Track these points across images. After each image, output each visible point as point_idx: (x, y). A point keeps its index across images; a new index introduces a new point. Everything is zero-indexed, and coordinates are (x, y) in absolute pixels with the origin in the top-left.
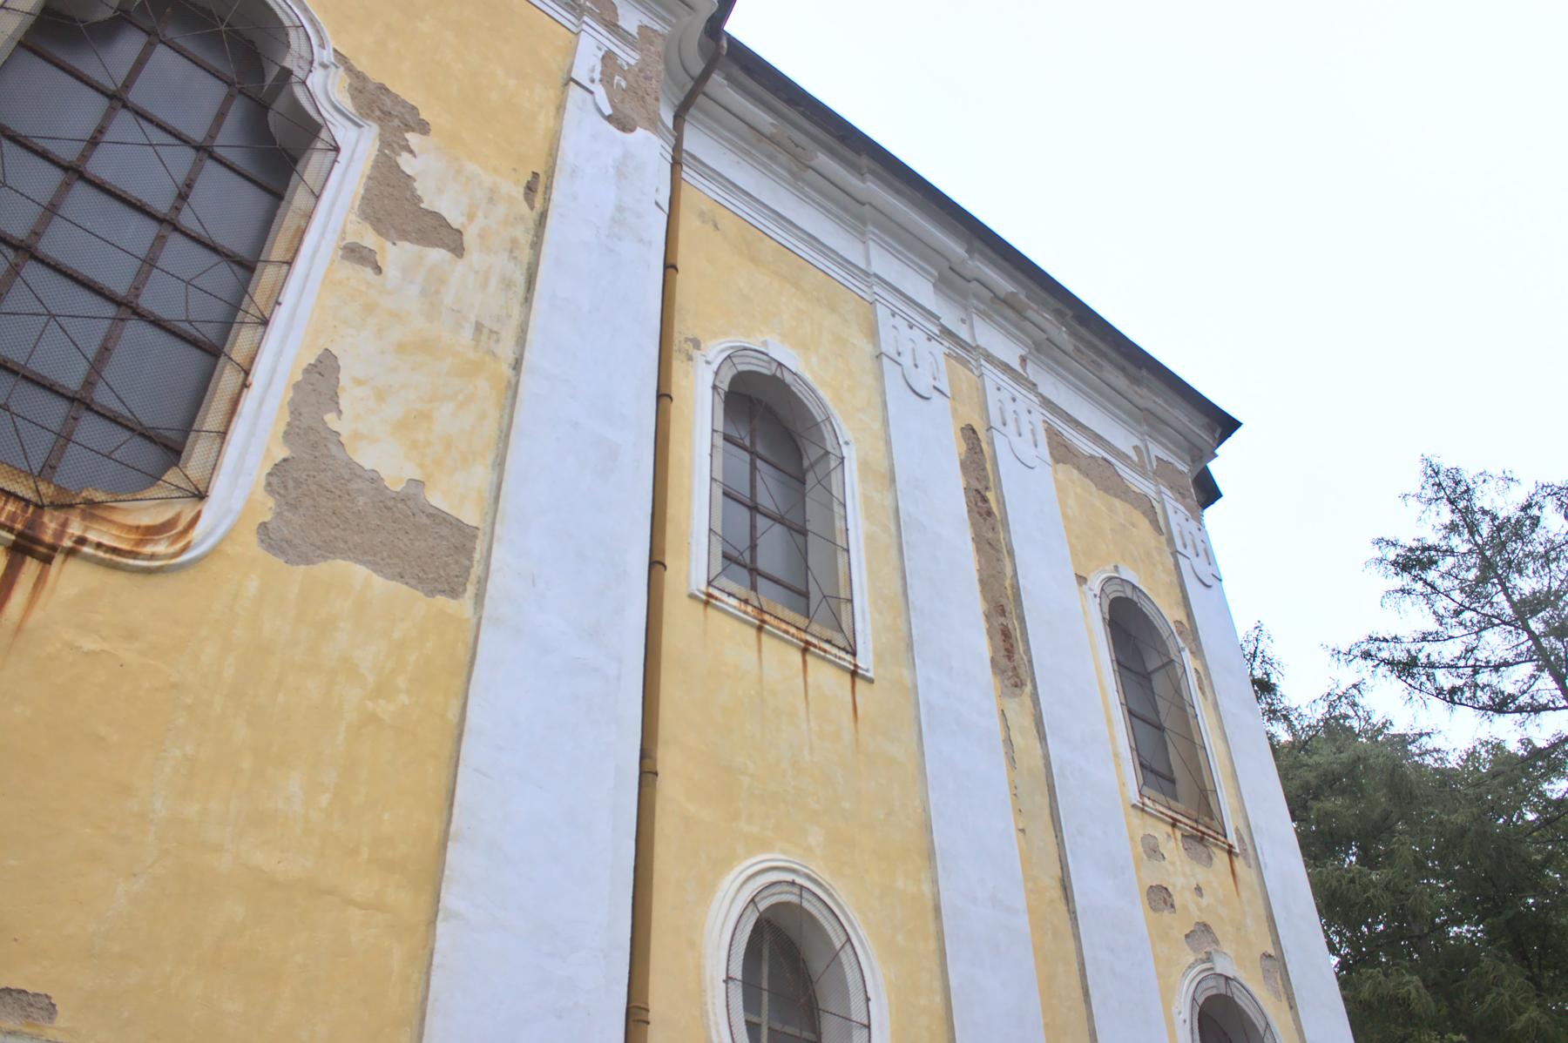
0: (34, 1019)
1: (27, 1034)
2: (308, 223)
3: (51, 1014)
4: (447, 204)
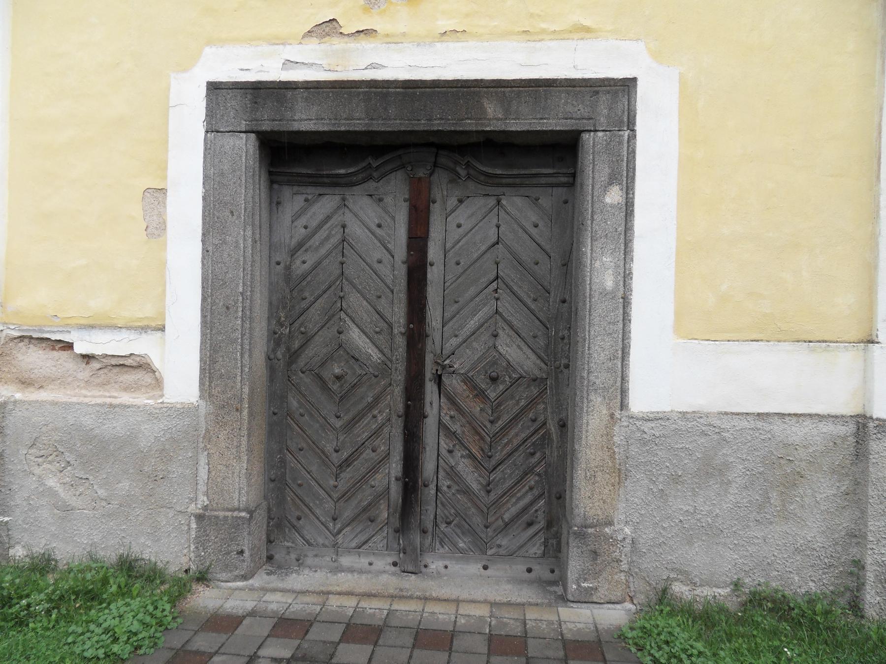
2: (574, 179)
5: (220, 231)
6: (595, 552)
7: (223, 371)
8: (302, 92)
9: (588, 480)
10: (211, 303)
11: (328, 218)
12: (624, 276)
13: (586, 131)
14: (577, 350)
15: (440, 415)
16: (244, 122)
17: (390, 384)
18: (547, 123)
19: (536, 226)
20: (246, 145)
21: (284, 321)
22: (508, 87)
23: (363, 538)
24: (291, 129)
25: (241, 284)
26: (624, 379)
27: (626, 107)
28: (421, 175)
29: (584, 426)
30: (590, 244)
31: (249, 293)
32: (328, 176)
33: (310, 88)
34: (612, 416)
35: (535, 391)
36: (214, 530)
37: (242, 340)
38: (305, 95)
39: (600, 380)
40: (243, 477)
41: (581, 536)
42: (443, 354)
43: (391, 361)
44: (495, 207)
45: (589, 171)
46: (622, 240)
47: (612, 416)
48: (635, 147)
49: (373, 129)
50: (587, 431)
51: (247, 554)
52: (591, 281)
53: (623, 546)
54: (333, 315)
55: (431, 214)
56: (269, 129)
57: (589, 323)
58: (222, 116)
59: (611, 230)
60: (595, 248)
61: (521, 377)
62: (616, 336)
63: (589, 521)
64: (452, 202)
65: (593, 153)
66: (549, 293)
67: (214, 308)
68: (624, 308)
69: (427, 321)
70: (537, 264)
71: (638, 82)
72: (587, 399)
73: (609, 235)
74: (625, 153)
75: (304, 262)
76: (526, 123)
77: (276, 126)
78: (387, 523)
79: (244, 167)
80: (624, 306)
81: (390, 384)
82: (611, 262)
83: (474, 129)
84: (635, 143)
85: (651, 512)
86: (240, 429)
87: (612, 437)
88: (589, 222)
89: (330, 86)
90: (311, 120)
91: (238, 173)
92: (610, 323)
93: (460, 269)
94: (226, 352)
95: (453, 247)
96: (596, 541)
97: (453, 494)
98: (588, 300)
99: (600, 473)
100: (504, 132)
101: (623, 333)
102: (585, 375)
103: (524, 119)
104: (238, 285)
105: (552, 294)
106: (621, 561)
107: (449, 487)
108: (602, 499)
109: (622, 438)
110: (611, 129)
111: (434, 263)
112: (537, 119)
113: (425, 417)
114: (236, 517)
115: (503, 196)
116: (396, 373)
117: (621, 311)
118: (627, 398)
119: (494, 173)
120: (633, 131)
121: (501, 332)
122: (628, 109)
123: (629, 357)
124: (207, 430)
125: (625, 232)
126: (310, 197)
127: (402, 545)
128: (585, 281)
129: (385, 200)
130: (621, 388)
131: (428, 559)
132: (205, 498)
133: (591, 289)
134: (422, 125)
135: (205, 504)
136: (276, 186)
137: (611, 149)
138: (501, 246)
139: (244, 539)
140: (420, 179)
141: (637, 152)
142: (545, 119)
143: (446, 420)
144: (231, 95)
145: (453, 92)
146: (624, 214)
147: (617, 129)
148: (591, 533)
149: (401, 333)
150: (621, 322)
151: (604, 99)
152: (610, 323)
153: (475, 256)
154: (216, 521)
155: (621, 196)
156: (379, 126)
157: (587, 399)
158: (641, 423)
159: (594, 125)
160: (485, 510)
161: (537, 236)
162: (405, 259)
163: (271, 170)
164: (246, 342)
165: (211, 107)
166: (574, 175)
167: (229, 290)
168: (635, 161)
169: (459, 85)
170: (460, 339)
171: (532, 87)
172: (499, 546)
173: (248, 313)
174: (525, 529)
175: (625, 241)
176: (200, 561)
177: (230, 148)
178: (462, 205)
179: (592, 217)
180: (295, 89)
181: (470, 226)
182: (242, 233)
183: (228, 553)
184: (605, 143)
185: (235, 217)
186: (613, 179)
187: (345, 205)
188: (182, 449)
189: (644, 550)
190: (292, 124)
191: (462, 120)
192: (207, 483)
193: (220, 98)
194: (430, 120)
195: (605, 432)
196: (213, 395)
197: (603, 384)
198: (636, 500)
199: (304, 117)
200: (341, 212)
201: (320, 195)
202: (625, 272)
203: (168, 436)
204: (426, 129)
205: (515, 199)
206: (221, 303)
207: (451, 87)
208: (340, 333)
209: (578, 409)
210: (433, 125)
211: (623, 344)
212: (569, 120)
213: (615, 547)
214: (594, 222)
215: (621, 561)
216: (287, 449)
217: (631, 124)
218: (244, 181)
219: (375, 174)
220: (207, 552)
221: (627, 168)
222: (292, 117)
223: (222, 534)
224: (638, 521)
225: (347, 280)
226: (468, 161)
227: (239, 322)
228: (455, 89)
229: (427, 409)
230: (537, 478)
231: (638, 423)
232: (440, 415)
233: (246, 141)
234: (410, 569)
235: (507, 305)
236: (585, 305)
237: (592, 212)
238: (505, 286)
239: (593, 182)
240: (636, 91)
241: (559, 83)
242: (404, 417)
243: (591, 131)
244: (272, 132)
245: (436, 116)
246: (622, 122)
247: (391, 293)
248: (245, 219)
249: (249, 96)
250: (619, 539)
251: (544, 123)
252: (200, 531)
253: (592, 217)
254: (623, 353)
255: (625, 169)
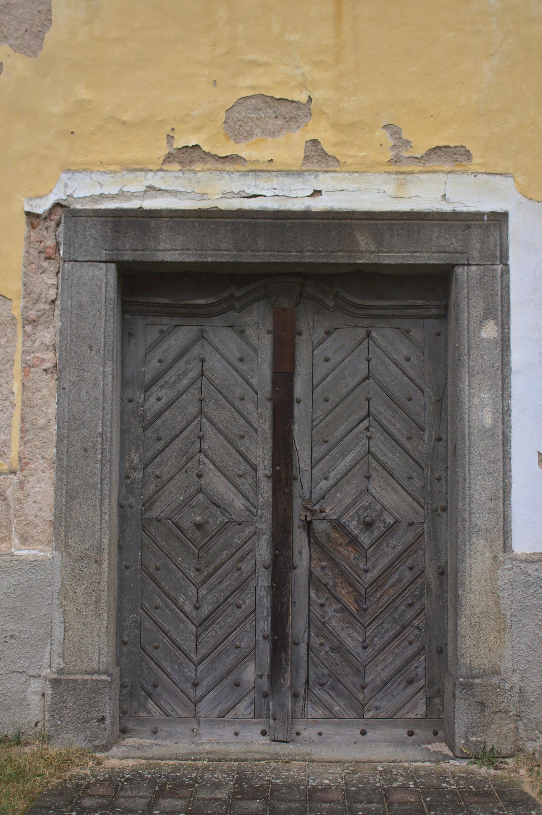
0: (459, 162)
1: (458, 171)
2: (446, 311)
3: (469, 157)
4: (386, 134)
5: (77, 367)
6: (482, 704)
7: (80, 519)
8: (167, 221)
9: (473, 628)
10: (67, 445)
11: (185, 351)
12: (503, 413)
13: (459, 265)
14: (458, 491)
15: (310, 566)
16: (105, 252)
17: (255, 533)
18: (420, 256)
19: (408, 360)
20: (106, 275)
21: (137, 464)
22: (380, 220)
23: (225, 706)
24: (155, 259)
25: (100, 424)
26: (506, 519)
27: (498, 241)
28: (286, 305)
29: (467, 570)
30: (467, 380)
31: (109, 434)
32: (186, 306)
33: (175, 217)
34: (495, 557)
35: (410, 537)
36: (72, 695)
37: (101, 485)
38: (170, 224)
39: (482, 521)
40: (103, 635)
41: (468, 687)
42: (313, 498)
43: (255, 507)
44: (364, 340)
45: (464, 305)
46: (499, 376)
47: (495, 557)
48: (509, 281)
49: (242, 261)
50: (470, 576)
51: (108, 721)
52: (469, 418)
53: (510, 695)
54: (192, 458)
55: (297, 348)
56: (131, 259)
57: (469, 462)
58: (81, 245)
59: (488, 366)
60: (472, 385)
61: (397, 522)
62: (496, 475)
63: (475, 672)
64: (319, 334)
65: (467, 287)
66: (424, 431)
67: (70, 450)
68: (503, 446)
69: (294, 462)
70: (410, 400)
71: (509, 217)
72: (470, 542)
73: (486, 371)
74: (499, 288)
75: (159, 399)
76: (399, 256)
77: (139, 256)
78: (254, 687)
79: (104, 299)
80: (503, 444)
81: (255, 533)
82: (489, 398)
83: (347, 261)
84: (509, 278)
85: (538, 659)
86: (99, 583)
87: (496, 581)
88: (466, 358)
89: (196, 216)
90: (177, 250)
91: (98, 305)
92: (490, 462)
93: (328, 406)
94: (84, 498)
95: (321, 383)
96: (483, 692)
97: (327, 653)
98: (467, 437)
99: (484, 620)
100: (377, 264)
101: (504, 471)
102: (467, 516)
103: (397, 252)
104: (97, 425)
105: (427, 431)
106: (510, 712)
107: (322, 645)
108: (488, 647)
109: (506, 581)
110: (484, 263)
111: (301, 400)
112: (410, 252)
113: (294, 568)
114: (97, 680)
115: (373, 328)
116: (261, 520)
117: (501, 449)
118: (510, 540)
119: (364, 304)
120: (506, 265)
121: (374, 474)
122: (501, 243)
123: (510, 497)
124: (63, 585)
125: (502, 368)
126: (165, 328)
127: (272, 711)
128: (463, 418)
129: (247, 332)
130: (504, 529)
131: (299, 727)
132: (61, 661)
133: (469, 427)
134: (293, 257)
135: (61, 667)
136: (128, 317)
137: (485, 283)
138: (372, 381)
139: (105, 704)
140: (284, 309)
141: (511, 286)
142: (418, 252)
143: (317, 572)
144: (91, 223)
145: (324, 224)
146: (500, 349)
147: (490, 263)
148: (478, 684)
149: (267, 477)
150: (501, 460)
151: (476, 234)
152: (490, 462)
153: (345, 391)
154: (74, 686)
155: (497, 331)
156: (247, 257)
157: (470, 542)
158: (524, 565)
159: (468, 259)
160: (362, 668)
161: (410, 370)
162: (269, 396)
163: (126, 299)
164: (106, 487)
165: (68, 235)
166: (446, 307)
167: (88, 431)
168: (509, 295)
169: (331, 217)
170: (331, 482)
171: (404, 220)
172: (377, 708)
173: (108, 456)
174: (406, 687)
175: (502, 377)
176: (56, 730)
177: (89, 279)
178: (330, 338)
179: (469, 352)
180: (160, 217)
181: (339, 359)
182: (101, 369)
183: (88, 721)
184: (479, 277)
185: (94, 352)
186: (488, 314)
187: (203, 337)
188: (34, 606)
189: (532, 699)
190: (156, 254)
191: (335, 252)
192: (63, 643)
193: (79, 226)
194: (301, 252)
195: (489, 576)
196: (69, 546)
197: (485, 526)
198: (523, 646)
199: (168, 247)
200: (200, 344)
201: (176, 326)
202: (503, 409)
203: (19, 592)
204: (296, 261)
205: (385, 331)
206: (79, 445)
207: (322, 219)
208: (199, 476)
209: (460, 552)
210: (303, 257)
211: (504, 483)
212: (442, 254)
213: (503, 697)
214: (471, 357)
215: (510, 712)
216: (142, 608)
217: (504, 258)
218: (103, 314)
219: (237, 305)
220: (64, 720)
221: (502, 303)
222: (155, 247)
223: (80, 699)
224: (525, 668)
225: (206, 418)
226: (337, 292)
227: (98, 466)
228: (326, 221)
229: (296, 560)
230: (416, 632)
231: (522, 566)
232: (310, 566)
233: (106, 271)
234: (281, 737)
235: (380, 444)
236: (464, 443)
237: (469, 347)
238: (376, 424)
239: (468, 316)
240: (508, 226)
241: (432, 217)
242: (271, 569)
243: (464, 265)
244: (134, 262)
245: (307, 248)
246: (495, 256)
247: (254, 432)
248: (104, 354)
249: (110, 225)
250: (507, 688)
251: (417, 257)
252: (56, 697)
253: (469, 352)
254: (504, 492)
255: (500, 303)
